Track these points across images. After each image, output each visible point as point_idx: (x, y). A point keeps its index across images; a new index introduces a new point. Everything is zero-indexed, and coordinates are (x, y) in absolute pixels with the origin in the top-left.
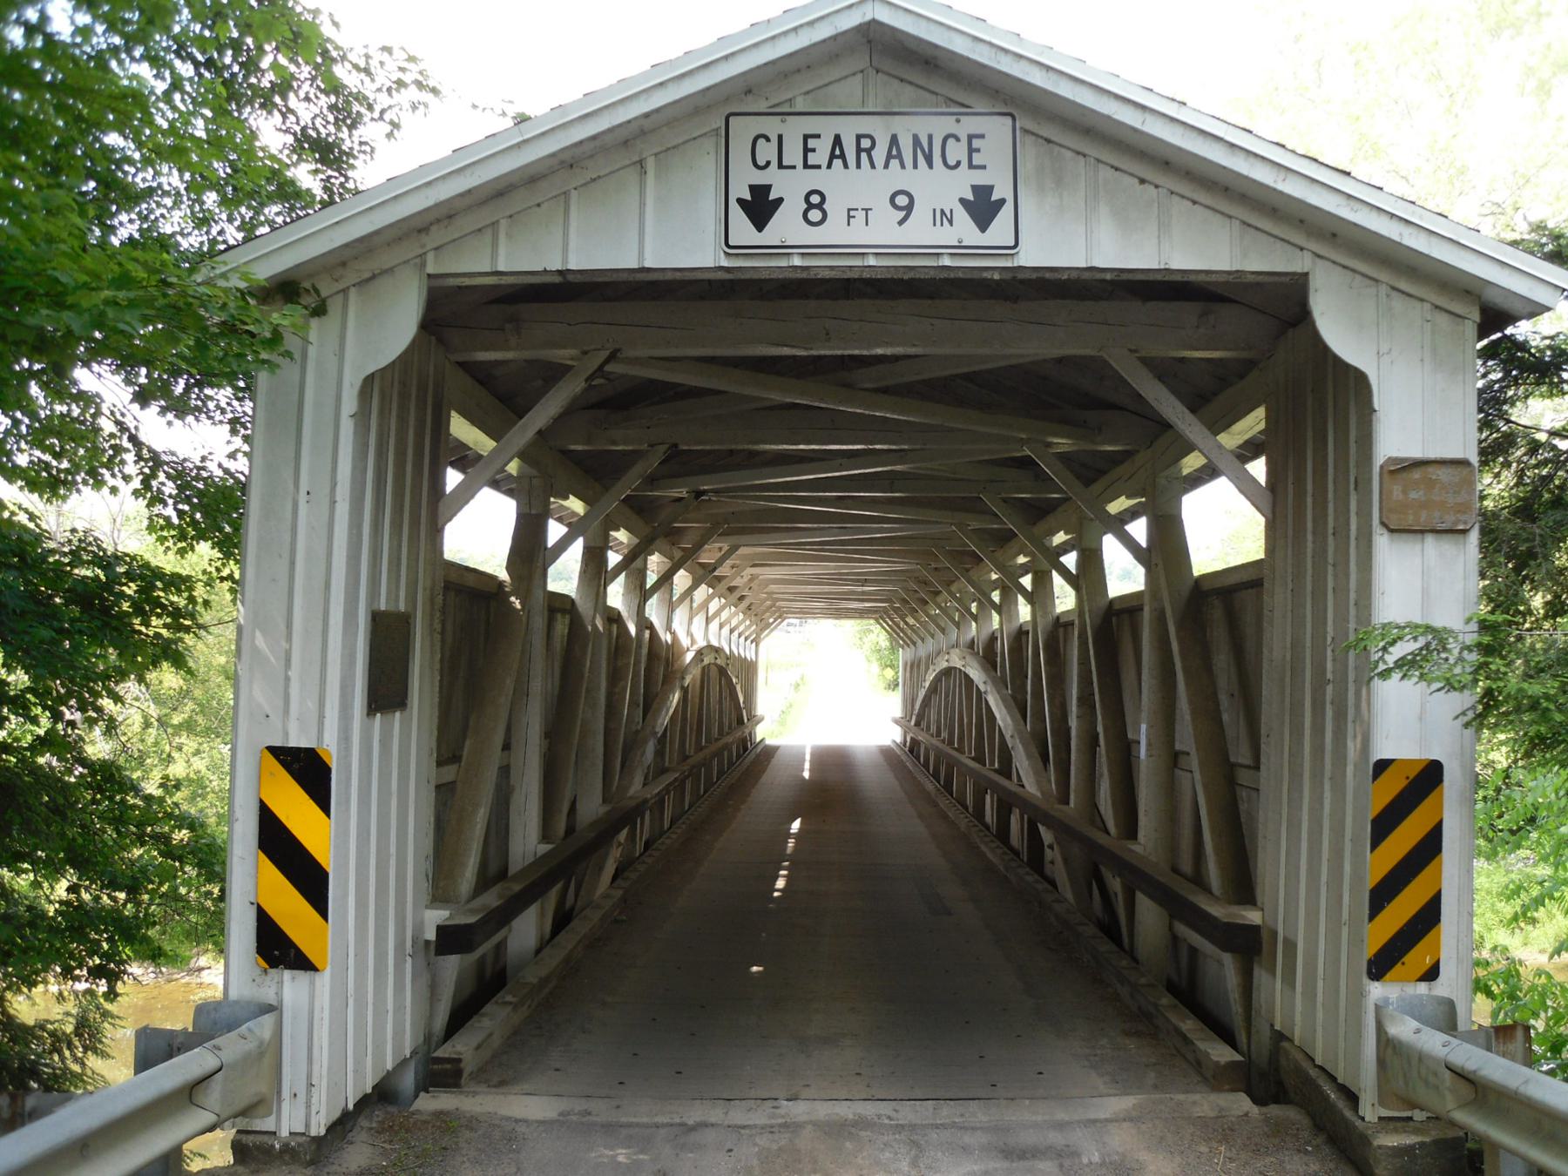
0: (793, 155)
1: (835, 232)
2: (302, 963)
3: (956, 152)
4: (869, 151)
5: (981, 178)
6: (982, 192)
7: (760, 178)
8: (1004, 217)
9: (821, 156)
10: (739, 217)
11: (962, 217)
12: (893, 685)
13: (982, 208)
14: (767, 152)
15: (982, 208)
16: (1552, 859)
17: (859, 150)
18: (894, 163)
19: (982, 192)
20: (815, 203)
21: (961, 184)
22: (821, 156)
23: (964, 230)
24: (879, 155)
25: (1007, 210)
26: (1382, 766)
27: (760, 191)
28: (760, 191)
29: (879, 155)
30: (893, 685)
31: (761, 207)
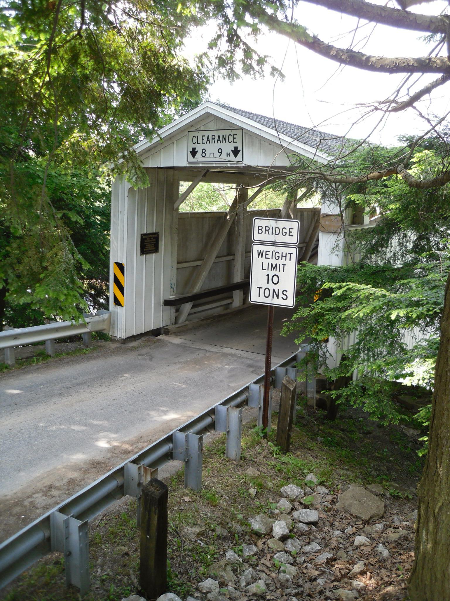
0: (200, 141)
3: (231, 139)
6: (236, 148)
7: (194, 146)
9: (205, 141)
10: (190, 154)
11: (232, 154)
14: (195, 140)
15: (236, 152)
19: (236, 148)
20: (204, 152)
21: (231, 147)
22: (205, 141)
23: (232, 157)
24: (216, 140)
27: (194, 149)
28: (194, 149)
29: (216, 140)
31: (194, 153)
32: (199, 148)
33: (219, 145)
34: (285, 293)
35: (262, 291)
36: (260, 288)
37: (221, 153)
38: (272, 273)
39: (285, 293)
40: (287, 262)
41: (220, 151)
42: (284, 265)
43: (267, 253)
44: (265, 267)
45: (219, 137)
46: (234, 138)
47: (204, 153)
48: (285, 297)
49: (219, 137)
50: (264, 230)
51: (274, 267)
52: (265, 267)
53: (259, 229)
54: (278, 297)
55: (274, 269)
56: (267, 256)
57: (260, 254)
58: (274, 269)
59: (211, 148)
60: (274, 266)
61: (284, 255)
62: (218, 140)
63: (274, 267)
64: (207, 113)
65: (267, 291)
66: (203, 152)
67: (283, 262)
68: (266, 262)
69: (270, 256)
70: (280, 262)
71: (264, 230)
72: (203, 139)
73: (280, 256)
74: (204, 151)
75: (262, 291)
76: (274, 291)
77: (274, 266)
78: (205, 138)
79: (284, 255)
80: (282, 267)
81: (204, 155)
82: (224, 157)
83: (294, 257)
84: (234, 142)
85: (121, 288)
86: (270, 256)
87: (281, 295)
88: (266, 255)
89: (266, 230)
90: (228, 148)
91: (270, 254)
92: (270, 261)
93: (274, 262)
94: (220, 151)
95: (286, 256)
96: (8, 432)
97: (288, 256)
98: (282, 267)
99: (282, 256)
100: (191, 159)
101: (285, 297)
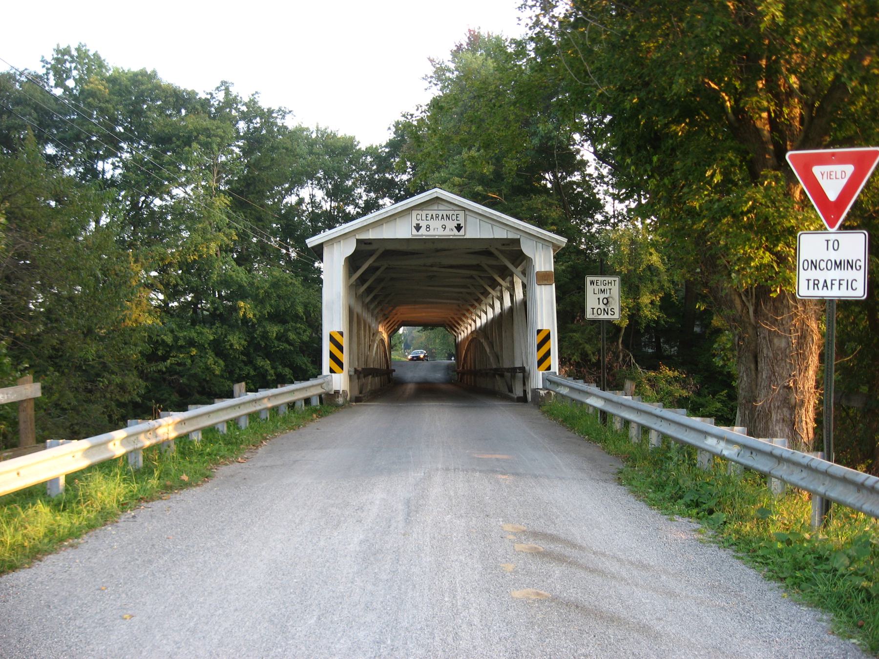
0: (424, 218)
1: (432, 233)
2: (335, 372)
3: (454, 217)
4: (817, 285)
5: (458, 222)
6: (459, 225)
7: (418, 222)
8: (463, 229)
9: (429, 218)
10: (414, 229)
11: (455, 230)
12: (104, 60)
13: (459, 228)
14: (419, 217)
15: (459, 228)
16: (250, 175)
17: (814, 284)
18: (825, 288)
19: (459, 225)
20: (428, 227)
21: (455, 223)
22: (429, 218)
23: (455, 232)
24: (440, 218)
25: (463, 228)
26: (539, 331)
27: (418, 225)
28: (418, 225)
29: (440, 218)
30: (104, 60)
31: (418, 228)
32: (423, 224)
36: (593, 309)
38: (602, 296)
40: (612, 287)
41: (428, 227)
44: (596, 291)
51: (603, 291)
52: (596, 291)
54: (607, 314)
55: (838, 267)
57: (592, 283)
58: (838, 267)
59: (433, 224)
60: (838, 263)
62: (824, 286)
63: (603, 291)
65: (599, 310)
67: (610, 287)
68: (597, 288)
69: (599, 284)
70: (607, 287)
77: (838, 263)
78: (429, 216)
80: (608, 291)
83: (617, 283)
86: (599, 284)
87: (610, 312)
90: (451, 224)
91: (599, 282)
92: (600, 287)
93: (603, 287)
96: (103, 413)
97: (613, 282)
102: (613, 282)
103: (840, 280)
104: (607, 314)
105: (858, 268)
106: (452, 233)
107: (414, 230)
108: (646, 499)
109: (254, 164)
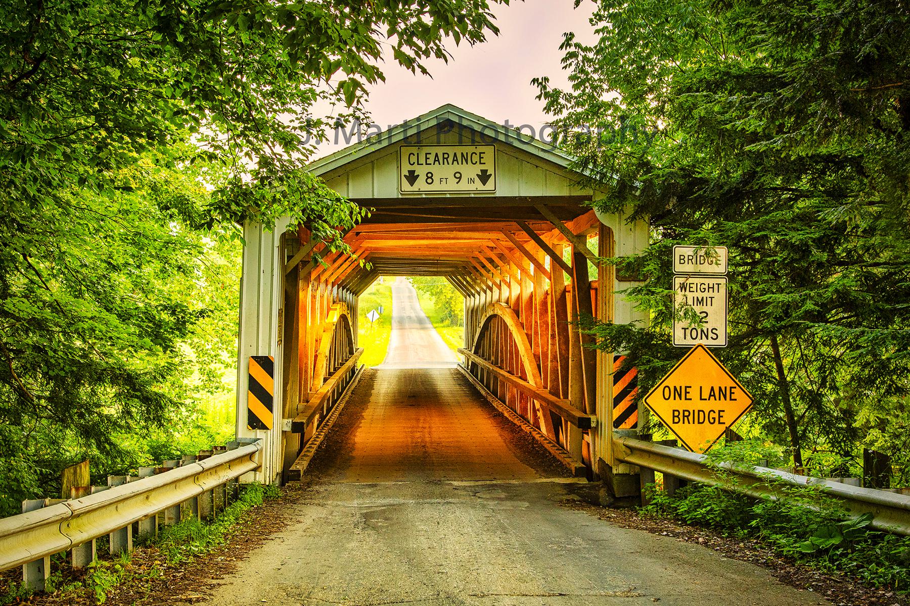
1: (436, 186)
3: (476, 158)
4: (447, 159)
5: (483, 167)
6: (484, 172)
7: (412, 168)
9: (431, 161)
10: (404, 180)
11: (477, 180)
13: (484, 177)
18: (712, 398)
19: (484, 172)
20: (430, 177)
21: (477, 169)
22: (431, 161)
23: (478, 185)
24: (450, 160)
27: (412, 172)
28: (412, 172)
29: (450, 160)
31: (412, 178)
32: (421, 171)
33: (456, 167)
34: (714, 331)
35: (688, 332)
37: (460, 178)
39: (714, 331)
40: (715, 294)
41: (458, 177)
42: (712, 298)
43: (691, 286)
45: (455, 154)
46: (481, 158)
47: (431, 178)
48: (715, 337)
49: (455, 154)
50: (686, 259)
53: (680, 259)
54: (707, 338)
56: (691, 290)
59: (438, 171)
61: (711, 286)
62: (454, 160)
64: (449, 120)
66: (428, 178)
67: (711, 294)
70: (705, 295)
71: (686, 259)
72: (427, 159)
73: (706, 287)
74: (430, 175)
75: (688, 332)
76: (702, 331)
78: (432, 158)
79: (711, 286)
80: (709, 300)
81: (430, 181)
82: (464, 186)
84: (480, 163)
85: (255, 387)
87: (710, 335)
88: (690, 287)
89: (688, 259)
91: (694, 286)
92: (695, 295)
93: (700, 295)
94: (458, 175)
95: (713, 288)
97: (716, 286)
98: (709, 300)
99: (709, 288)
100: (406, 186)
101: (715, 337)
102: (716, 286)
103: (720, 411)
104: (707, 338)
105: (712, 421)
106: (472, 187)
107: (405, 183)
108: (796, 498)
109: (32, 117)
